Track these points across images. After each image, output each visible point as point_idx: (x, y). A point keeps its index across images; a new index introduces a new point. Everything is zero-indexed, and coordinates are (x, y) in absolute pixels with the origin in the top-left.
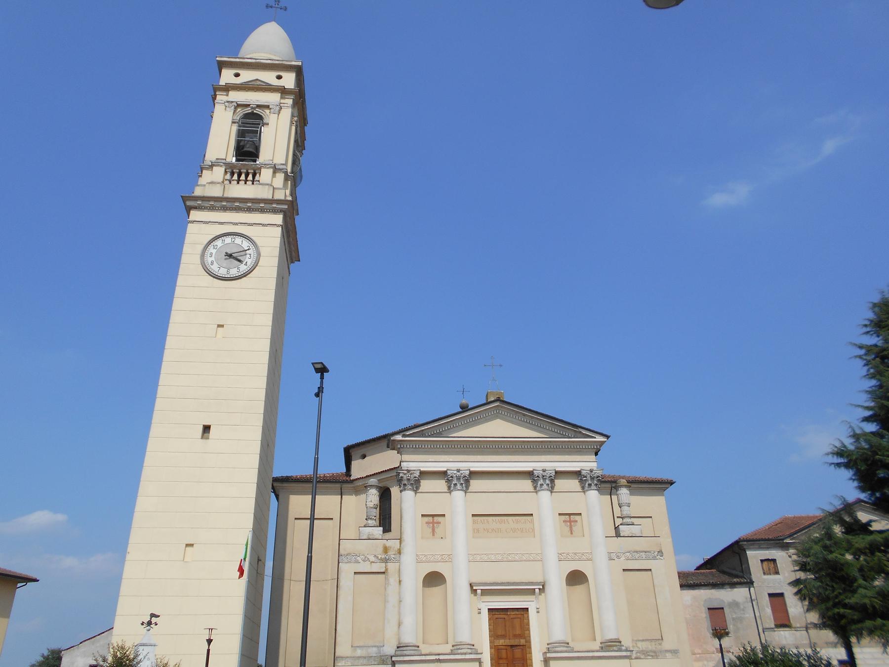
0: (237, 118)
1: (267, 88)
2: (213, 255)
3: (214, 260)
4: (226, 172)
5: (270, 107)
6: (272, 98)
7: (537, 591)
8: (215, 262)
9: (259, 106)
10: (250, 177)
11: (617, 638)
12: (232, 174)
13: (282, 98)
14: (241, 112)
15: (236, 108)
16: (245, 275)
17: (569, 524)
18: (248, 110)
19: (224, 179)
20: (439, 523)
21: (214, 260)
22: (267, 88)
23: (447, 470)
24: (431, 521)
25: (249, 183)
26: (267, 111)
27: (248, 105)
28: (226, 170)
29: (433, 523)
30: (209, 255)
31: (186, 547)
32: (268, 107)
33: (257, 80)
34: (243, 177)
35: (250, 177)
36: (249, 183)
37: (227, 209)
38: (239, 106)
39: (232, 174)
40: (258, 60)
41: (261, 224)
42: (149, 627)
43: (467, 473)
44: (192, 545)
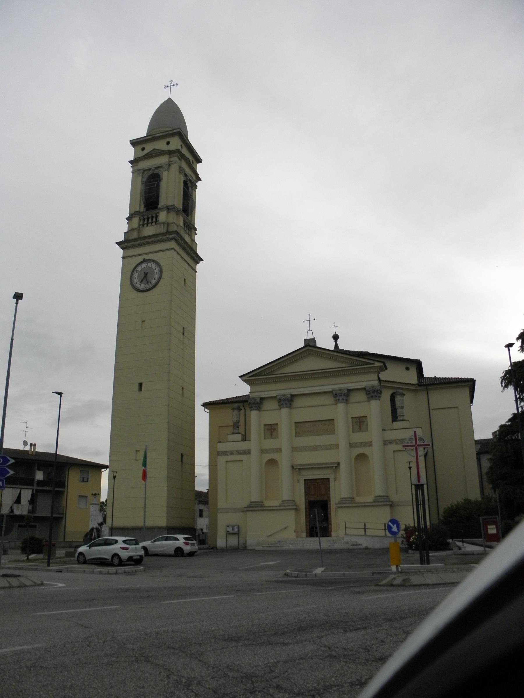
0: (145, 179)
1: (160, 153)
2: (137, 277)
3: (137, 280)
4: (140, 219)
5: (163, 166)
6: (163, 160)
7: (334, 467)
8: (138, 282)
9: (156, 168)
10: (154, 220)
11: (259, 500)
12: (144, 219)
13: (170, 158)
14: (147, 174)
15: (143, 173)
16: (155, 286)
17: (359, 423)
18: (151, 172)
19: (140, 225)
20: (275, 429)
21: (137, 280)
22: (160, 153)
23: (277, 395)
24: (359, 421)
25: (154, 224)
26: (161, 169)
27: (150, 169)
28: (140, 218)
29: (360, 422)
30: (134, 278)
31: (136, 453)
32: (161, 167)
33: (154, 149)
34: (150, 221)
35: (154, 220)
36: (145, 225)
37: (130, 248)
38: (144, 171)
39: (144, 219)
40: (154, 136)
41: (161, 250)
42: (95, 496)
43: (289, 396)
44: (139, 451)
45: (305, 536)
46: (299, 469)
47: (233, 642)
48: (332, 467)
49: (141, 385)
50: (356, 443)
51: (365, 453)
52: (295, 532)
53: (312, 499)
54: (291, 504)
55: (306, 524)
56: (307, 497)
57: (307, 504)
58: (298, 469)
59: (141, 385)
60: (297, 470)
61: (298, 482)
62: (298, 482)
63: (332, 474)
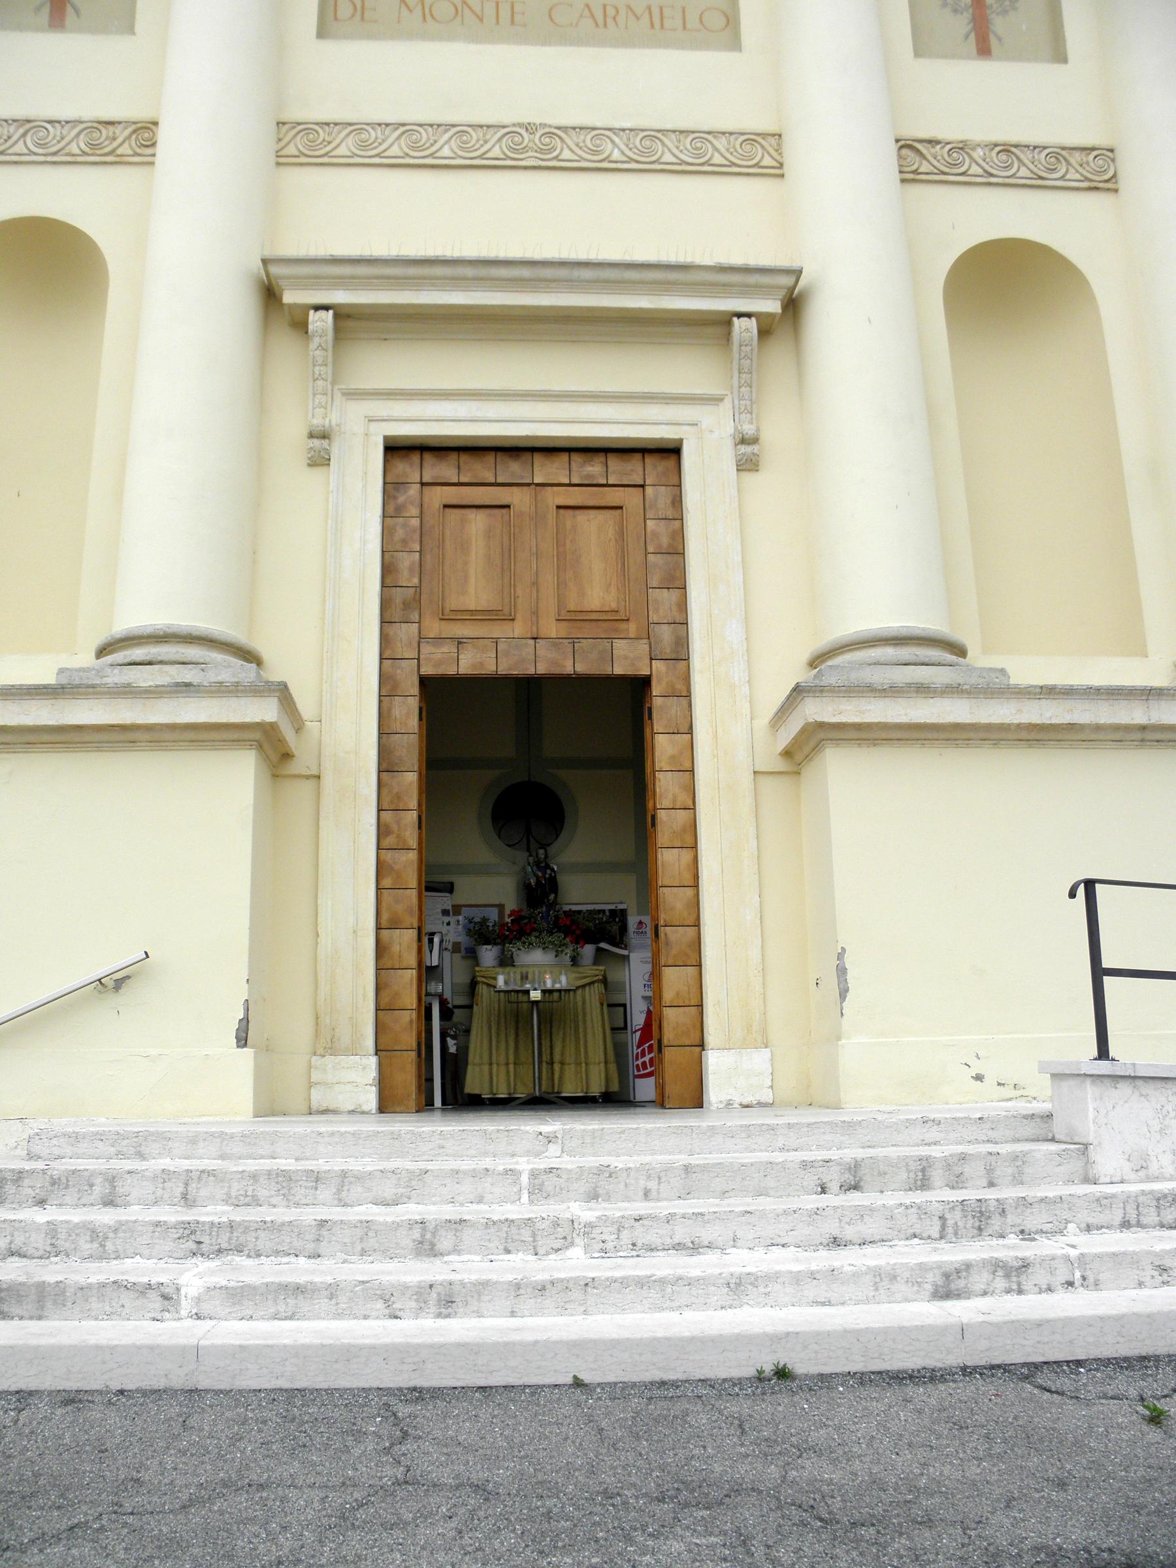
7: (744, 329)
45: (370, 1099)
46: (343, 315)
47: (120, 1190)
48: (724, 321)
49: (999, 1084)
50: (963, 147)
51: (1055, 246)
52: (242, 1040)
53: (468, 663)
54: (212, 676)
55: (381, 949)
56: (406, 633)
57: (408, 710)
58: (640, 1096)
59: (999, 1084)
60: (321, 322)
61: (320, 461)
62: (320, 461)
63: (716, 400)
